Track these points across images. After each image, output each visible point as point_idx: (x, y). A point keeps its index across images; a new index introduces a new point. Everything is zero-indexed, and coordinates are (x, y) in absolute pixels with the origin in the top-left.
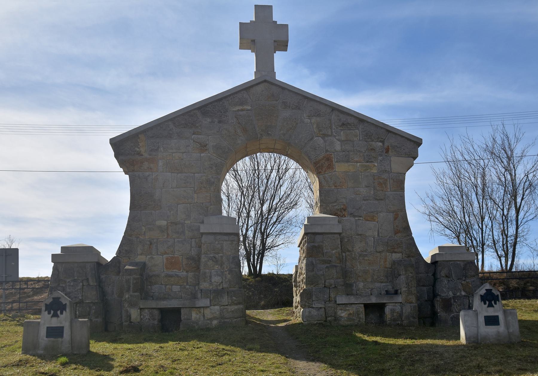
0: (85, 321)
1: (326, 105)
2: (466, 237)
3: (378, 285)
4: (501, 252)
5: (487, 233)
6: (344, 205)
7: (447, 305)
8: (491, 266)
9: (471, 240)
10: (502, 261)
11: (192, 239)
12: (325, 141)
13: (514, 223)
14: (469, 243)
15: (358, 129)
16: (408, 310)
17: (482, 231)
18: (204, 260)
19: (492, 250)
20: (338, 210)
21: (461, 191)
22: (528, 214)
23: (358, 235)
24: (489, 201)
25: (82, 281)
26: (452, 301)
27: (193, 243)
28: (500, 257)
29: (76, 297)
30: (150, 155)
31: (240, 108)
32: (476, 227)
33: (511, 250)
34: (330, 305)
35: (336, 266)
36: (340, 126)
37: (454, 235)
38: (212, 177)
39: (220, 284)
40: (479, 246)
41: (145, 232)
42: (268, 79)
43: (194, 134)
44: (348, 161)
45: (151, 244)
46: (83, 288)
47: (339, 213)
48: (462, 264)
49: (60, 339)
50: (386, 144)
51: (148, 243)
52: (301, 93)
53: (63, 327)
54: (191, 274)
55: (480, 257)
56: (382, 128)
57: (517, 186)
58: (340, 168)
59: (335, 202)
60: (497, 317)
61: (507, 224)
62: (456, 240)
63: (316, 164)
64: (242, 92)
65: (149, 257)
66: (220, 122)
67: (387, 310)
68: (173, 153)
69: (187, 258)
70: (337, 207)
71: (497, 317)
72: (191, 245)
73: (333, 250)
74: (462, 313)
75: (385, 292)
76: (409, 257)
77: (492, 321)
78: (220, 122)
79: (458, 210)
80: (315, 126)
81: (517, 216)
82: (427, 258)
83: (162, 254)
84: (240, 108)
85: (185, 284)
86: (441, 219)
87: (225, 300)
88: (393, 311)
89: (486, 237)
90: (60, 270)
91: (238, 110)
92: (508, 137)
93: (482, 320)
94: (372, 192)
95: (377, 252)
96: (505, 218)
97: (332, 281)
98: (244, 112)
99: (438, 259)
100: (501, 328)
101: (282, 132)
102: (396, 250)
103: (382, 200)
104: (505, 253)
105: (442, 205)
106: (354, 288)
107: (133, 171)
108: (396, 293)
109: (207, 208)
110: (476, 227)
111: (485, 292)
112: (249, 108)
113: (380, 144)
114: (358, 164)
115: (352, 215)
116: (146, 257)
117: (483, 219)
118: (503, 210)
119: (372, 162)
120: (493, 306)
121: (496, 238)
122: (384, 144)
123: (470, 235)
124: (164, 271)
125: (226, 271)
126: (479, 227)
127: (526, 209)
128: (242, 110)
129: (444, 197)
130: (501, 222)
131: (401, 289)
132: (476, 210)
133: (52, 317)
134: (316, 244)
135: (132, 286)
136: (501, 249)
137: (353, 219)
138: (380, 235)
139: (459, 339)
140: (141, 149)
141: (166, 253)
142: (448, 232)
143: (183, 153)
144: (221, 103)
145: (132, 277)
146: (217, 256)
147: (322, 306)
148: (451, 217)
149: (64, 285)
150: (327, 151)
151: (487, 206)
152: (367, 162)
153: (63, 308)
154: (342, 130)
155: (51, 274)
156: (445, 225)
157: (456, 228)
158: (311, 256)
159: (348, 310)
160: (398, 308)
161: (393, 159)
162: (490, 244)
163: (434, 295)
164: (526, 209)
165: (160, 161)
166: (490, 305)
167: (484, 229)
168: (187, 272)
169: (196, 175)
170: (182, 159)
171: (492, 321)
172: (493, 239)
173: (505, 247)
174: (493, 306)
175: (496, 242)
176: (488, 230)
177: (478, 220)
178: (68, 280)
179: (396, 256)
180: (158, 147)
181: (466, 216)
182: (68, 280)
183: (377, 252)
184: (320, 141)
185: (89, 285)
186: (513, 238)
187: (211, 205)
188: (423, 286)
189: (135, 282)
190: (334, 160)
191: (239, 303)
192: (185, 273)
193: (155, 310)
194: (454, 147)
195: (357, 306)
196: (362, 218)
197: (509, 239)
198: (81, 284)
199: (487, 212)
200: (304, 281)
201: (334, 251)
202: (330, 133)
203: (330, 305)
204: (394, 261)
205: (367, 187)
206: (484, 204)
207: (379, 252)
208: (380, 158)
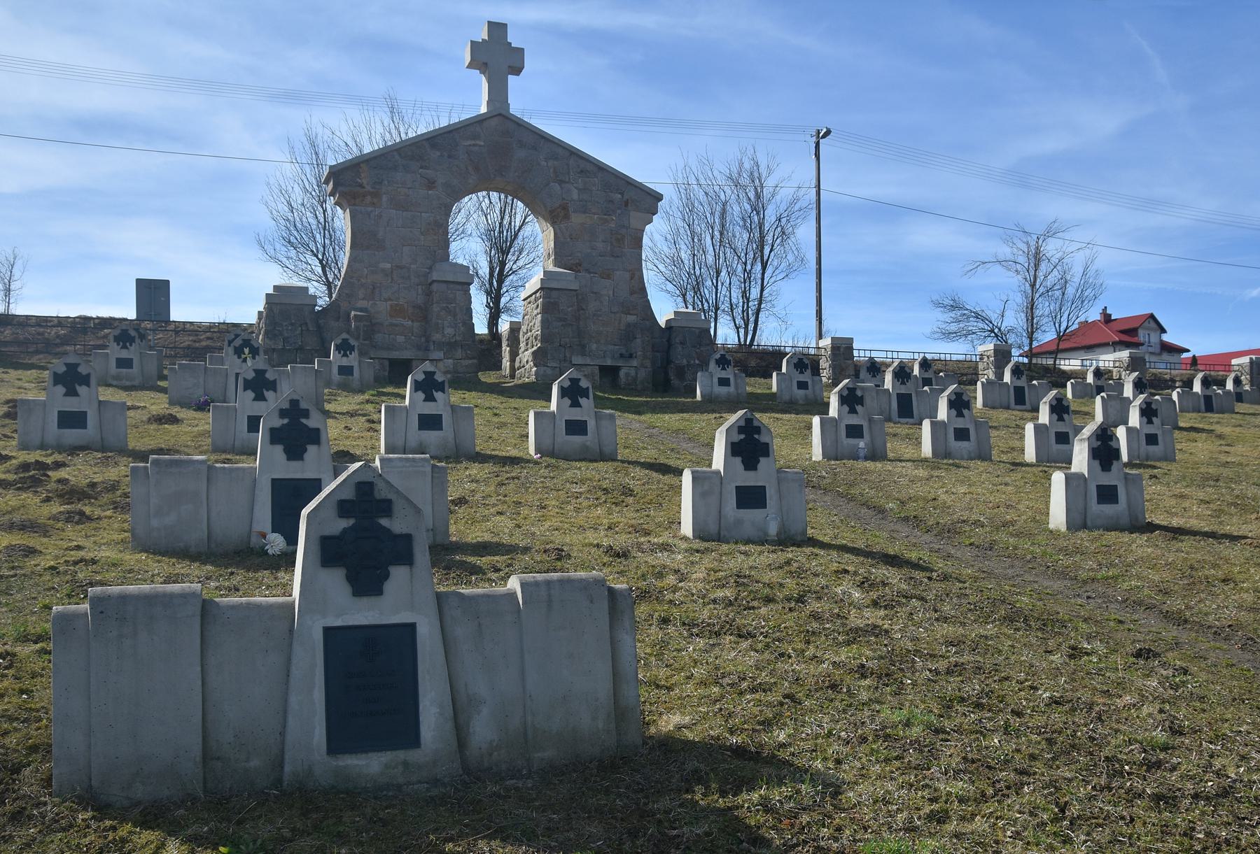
0: (371, 362)
1: (564, 148)
2: (694, 297)
3: (611, 347)
4: (739, 321)
5: (723, 293)
6: (579, 260)
7: (681, 372)
8: (726, 339)
9: (702, 302)
10: (740, 334)
11: (418, 285)
12: (562, 188)
13: (759, 282)
14: (698, 305)
15: (597, 177)
16: (642, 374)
17: (717, 290)
18: (436, 310)
19: (729, 318)
20: (574, 264)
21: (693, 233)
22: (777, 272)
23: (593, 293)
24: (728, 250)
25: (301, 326)
26: (686, 369)
27: (420, 291)
28: (737, 328)
29: (295, 343)
30: (372, 188)
31: (473, 142)
32: (709, 283)
33: (752, 319)
34: (565, 365)
35: (572, 325)
36: (579, 173)
37: (678, 292)
38: (441, 219)
39: (453, 336)
40: (712, 311)
41: (367, 274)
42: (504, 112)
43: (421, 168)
44: (585, 212)
45: (374, 288)
46: (302, 334)
47: (574, 268)
48: (697, 331)
49: (350, 377)
50: (626, 197)
51: (371, 287)
52: (537, 131)
53: (353, 367)
54: (416, 324)
55: (713, 325)
56: (623, 179)
57: (766, 232)
58: (577, 219)
59: (570, 256)
60: (729, 379)
61: (750, 284)
62: (680, 299)
63: (551, 212)
64: (475, 125)
65: (371, 302)
66: (450, 157)
67: (622, 373)
68: (398, 187)
69: (414, 307)
70: (572, 261)
71: (729, 379)
72: (417, 292)
73: (568, 307)
74: (699, 374)
75: (619, 355)
76: (644, 319)
77: (724, 382)
78: (450, 157)
79: (685, 255)
80: (551, 170)
81: (763, 274)
82: (662, 323)
83: (386, 300)
84: (473, 142)
85: (410, 335)
86: (661, 267)
87: (459, 353)
88: (627, 375)
89: (722, 298)
90: (275, 312)
91: (470, 145)
92: (758, 166)
93: (716, 381)
94: (609, 248)
95: (611, 312)
96: (747, 279)
97: (567, 340)
98: (477, 148)
99: (673, 324)
100: (732, 389)
101: (517, 174)
102: (631, 312)
103: (618, 257)
104: (744, 323)
105: (666, 249)
106: (587, 349)
107: (354, 205)
108: (631, 356)
109: (435, 252)
110: (709, 283)
111: (719, 356)
112: (482, 143)
113: (620, 196)
114: (596, 216)
115: (588, 271)
116: (368, 302)
117: (718, 273)
118: (745, 264)
119: (609, 215)
120: (726, 370)
121: (734, 301)
122: (623, 196)
123: (701, 294)
124: (387, 320)
125: (459, 323)
126: (713, 284)
127: (775, 263)
128: (474, 145)
129: (669, 237)
130: (742, 281)
131: (636, 353)
132: (710, 259)
133: (342, 356)
134: (552, 301)
135: (362, 334)
136: (739, 317)
137: (588, 275)
138: (615, 294)
139: (696, 397)
140: (363, 181)
141: (390, 299)
142: (670, 287)
143: (409, 188)
144: (452, 135)
145: (362, 324)
146: (450, 307)
147: (558, 366)
148: (675, 266)
149: (281, 329)
150: (563, 199)
151: (725, 255)
152: (605, 215)
153: (352, 349)
154: (579, 177)
155: (105, 316)
156: (666, 276)
157: (682, 282)
158: (546, 313)
159: (584, 371)
160: (633, 372)
161: (632, 214)
162: (726, 309)
163: (668, 361)
164: (776, 264)
165: (384, 196)
166: (724, 369)
167: (719, 287)
168: (412, 321)
169: (423, 214)
170: (408, 196)
171: (724, 382)
172: (731, 301)
173: (745, 314)
174: (726, 370)
175: (735, 307)
176: (724, 289)
177: (712, 273)
178: (285, 324)
179: (631, 319)
180: (382, 180)
181: (697, 267)
182: (285, 324)
183: (611, 312)
184: (557, 187)
185: (308, 330)
186: (756, 303)
187: (439, 249)
188: (657, 351)
189: (365, 329)
190: (571, 210)
191: (474, 358)
192: (410, 323)
193: (385, 360)
194: (688, 169)
195: (592, 367)
196: (597, 275)
197: (750, 304)
198: (300, 328)
199: (725, 264)
200: (539, 338)
201: (570, 309)
202: (567, 180)
203: (565, 365)
204: (629, 324)
205: (603, 242)
206: (721, 252)
207: (614, 313)
208: (619, 211)
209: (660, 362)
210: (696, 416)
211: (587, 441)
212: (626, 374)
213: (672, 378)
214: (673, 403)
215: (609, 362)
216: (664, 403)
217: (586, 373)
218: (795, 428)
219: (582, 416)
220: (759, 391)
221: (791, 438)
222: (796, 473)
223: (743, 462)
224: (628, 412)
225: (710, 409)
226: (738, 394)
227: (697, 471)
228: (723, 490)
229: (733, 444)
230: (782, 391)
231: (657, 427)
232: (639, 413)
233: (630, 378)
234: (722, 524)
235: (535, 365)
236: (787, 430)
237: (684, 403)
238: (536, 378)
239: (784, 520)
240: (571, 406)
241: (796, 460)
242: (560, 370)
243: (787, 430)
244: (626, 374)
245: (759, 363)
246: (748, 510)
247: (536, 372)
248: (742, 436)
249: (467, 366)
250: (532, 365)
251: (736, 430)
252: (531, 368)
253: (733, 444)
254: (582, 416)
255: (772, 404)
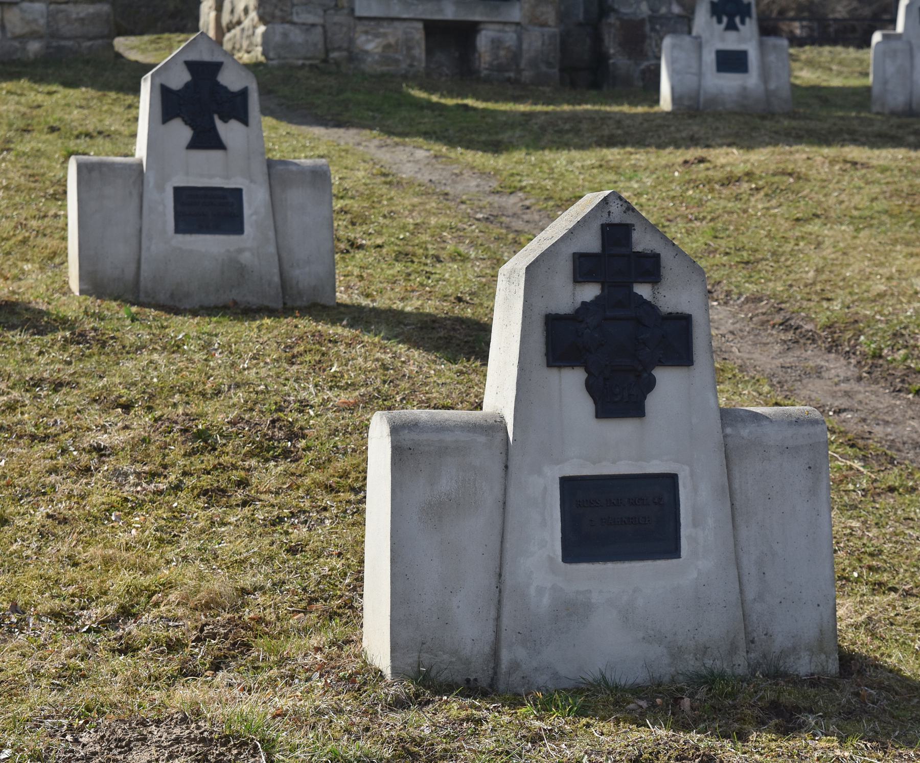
26: (647, 28)
67: (483, 41)
88: (496, 44)
93: (709, 58)
100: (752, 80)
159: (385, 35)
160: (510, 37)
166: (731, 27)
195: (405, 24)
203: (337, 19)
209: (582, 10)
210: (641, 157)
211: (240, 251)
212: (493, 41)
213: (612, 51)
214: (591, 118)
215: (450, 13)
216: (574, 118)
217: (392, 40)
218: (897, 193)
219: (227, 177)
220: (836, 82)
221: (882, 223)
222: (798, 422)
223: (591, 387)
224: (469, 145)
225: (684, 134)
226: (767, 90)
227: (414, 426)
228: (512, 491)
229: (553, 322)
230: (885, 82)
231: (522, 189)
232: (496, 147)
233: (502, 53)
234: (506, 621)
235: (263, 19)
236: (874, 199)
237: (620, 120)
238: (264, 53)
239: (750, 595)
240: (193, 145)
241: (881, 295)
242: (325, 32)
243: (874, 199)
244: (493, 41)
245: (855, 9)
246: (610, 565)
247: (265, 35)
248: (590, 292)
249: (82, 20)
250: (256, 19)
251: (565, 268)
252: (255, 27)
253: (553, 322)
254: (227, 177)
255: (857, 118)
